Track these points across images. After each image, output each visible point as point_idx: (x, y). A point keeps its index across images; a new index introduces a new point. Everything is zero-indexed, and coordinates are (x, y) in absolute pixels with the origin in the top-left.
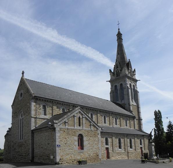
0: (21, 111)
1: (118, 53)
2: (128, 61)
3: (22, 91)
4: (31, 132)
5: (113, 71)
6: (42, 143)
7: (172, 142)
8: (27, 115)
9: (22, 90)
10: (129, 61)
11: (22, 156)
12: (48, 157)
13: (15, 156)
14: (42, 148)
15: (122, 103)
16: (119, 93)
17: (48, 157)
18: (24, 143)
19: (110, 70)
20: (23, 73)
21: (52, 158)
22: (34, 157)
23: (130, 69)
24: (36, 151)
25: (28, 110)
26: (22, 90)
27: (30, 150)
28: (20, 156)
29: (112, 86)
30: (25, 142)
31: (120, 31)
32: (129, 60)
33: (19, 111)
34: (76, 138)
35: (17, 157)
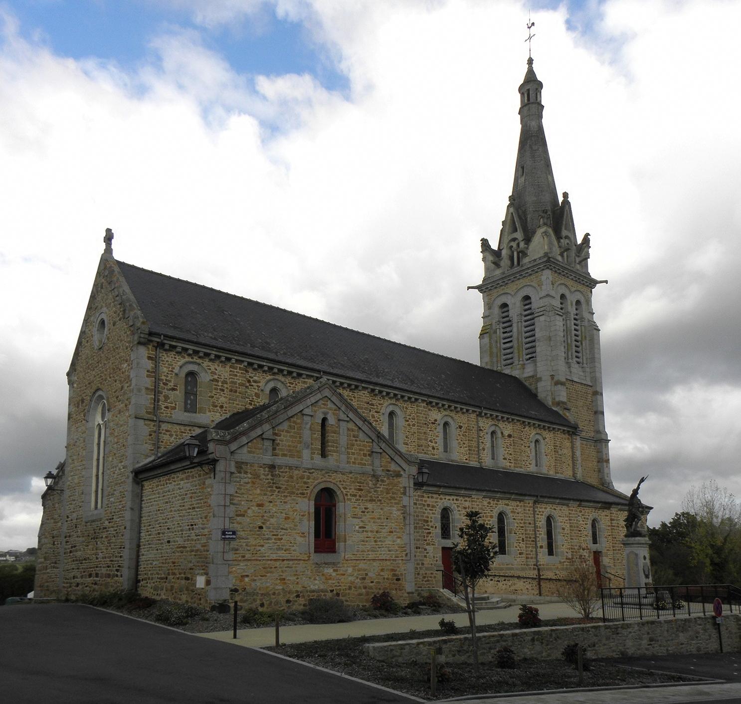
0: (100, 393)
1: (521, 168)
2: (561, 199)
3: (106, 314)
4: (131, 479)
5: (494, 246)
6: (169, 524)
7: (706, 562)
8: (120, 412)
9: (104, 309)
10: (566, 202)
11: (97, 575)
12: (187, 579)
13: (74, 577)
14: (169, 542)
15: (526, 375)
16: (516, 346)
17: (187, 579)
18: (107, 522)
19: (485, 243)
20: (109, 237)
21: (203, 586)
22: (138, 581)
23: (564, 233)
24: (147, 555)
25: (122, 387)
26: (104, 309)
27: (126, 553)
28: (90, 576)
29: (488, 306)
30: (110, 520)
31: (535, 66)
32: (565, 195)
33: (94, 393)
34: (307, 506)
35: (78, 580)
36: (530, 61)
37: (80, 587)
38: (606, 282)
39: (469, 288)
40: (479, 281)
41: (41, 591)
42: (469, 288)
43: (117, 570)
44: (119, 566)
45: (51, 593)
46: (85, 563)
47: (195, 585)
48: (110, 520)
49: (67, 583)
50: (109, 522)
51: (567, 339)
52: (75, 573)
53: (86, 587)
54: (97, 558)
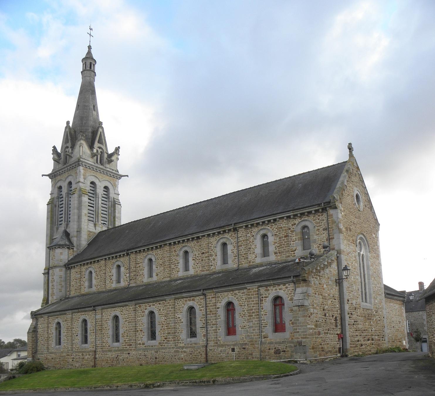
5: (59, 150)
11: (373, 340)
13: (358, 341)
17: (400, 342)
28: (368, 340)
29: (53, 186)
30: (376, 312)
31: (92, 51)
36: (90, 47)
37: (364, 346)
38: (127, 176)
39: (43, 175)
40: (50, 171)
41: (315, 352)
42: (43, 175)
43: (383, 338)
44: (383, 336)
45: (327, 353)
46: (365, 332)
47: (403, 344)
48: (376, 312)
49: (353, 344)
50: (376, 313)
51: (68, 209)
52: (358, 338)
53: (368, 346)
54: (371, 331)
